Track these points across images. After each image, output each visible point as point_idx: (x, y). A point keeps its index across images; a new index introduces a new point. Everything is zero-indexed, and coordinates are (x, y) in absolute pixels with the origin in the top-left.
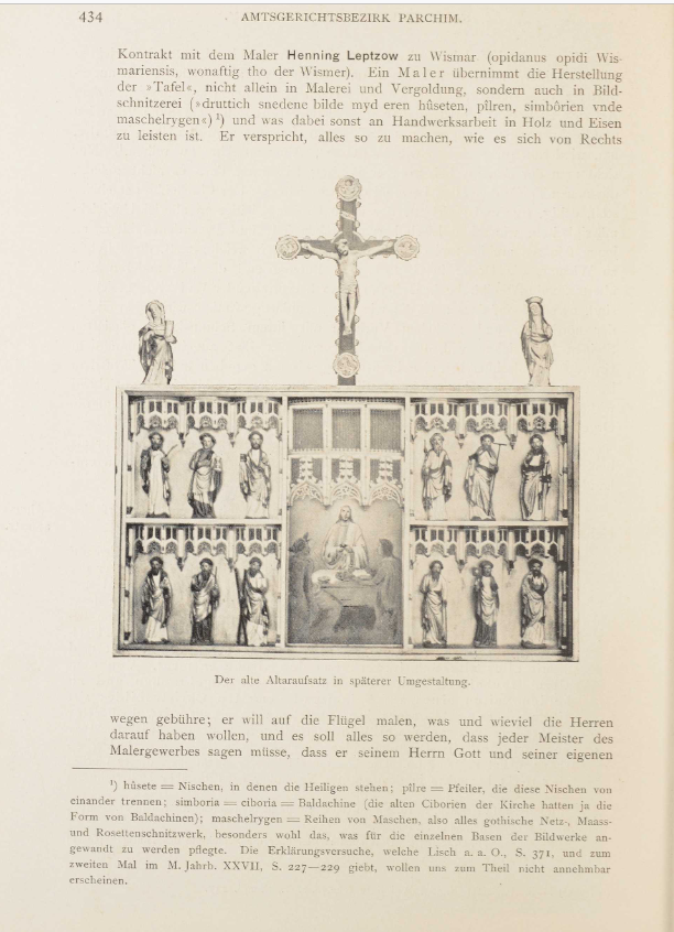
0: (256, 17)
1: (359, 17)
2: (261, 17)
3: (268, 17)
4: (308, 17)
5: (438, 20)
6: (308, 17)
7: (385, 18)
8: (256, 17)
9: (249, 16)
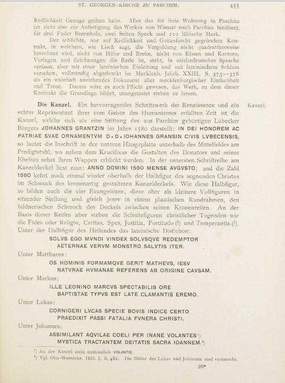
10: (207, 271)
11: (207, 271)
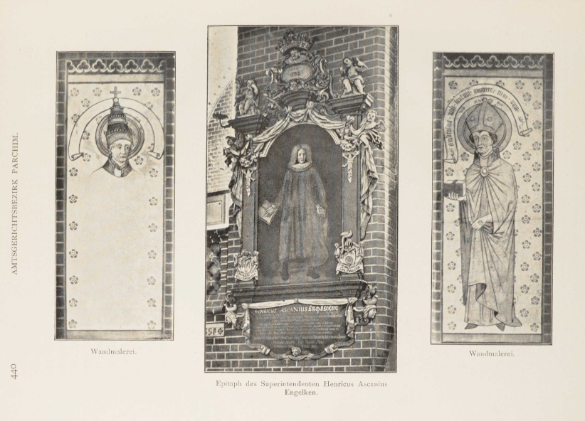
0: (14, 265)
1: (15, 199)
2: (14, 262)
3: (15, 257)
4: (14, 232)
5: (16, 149)
6: (14, 232)
7: (15, 183)
8: (14, 265)
9: (14, 269)
10: (15, 138)
11: (15, 138)
